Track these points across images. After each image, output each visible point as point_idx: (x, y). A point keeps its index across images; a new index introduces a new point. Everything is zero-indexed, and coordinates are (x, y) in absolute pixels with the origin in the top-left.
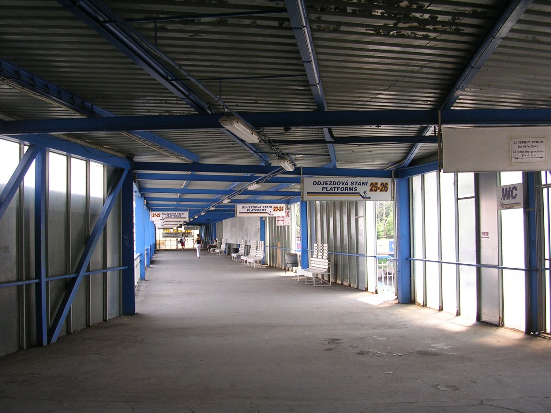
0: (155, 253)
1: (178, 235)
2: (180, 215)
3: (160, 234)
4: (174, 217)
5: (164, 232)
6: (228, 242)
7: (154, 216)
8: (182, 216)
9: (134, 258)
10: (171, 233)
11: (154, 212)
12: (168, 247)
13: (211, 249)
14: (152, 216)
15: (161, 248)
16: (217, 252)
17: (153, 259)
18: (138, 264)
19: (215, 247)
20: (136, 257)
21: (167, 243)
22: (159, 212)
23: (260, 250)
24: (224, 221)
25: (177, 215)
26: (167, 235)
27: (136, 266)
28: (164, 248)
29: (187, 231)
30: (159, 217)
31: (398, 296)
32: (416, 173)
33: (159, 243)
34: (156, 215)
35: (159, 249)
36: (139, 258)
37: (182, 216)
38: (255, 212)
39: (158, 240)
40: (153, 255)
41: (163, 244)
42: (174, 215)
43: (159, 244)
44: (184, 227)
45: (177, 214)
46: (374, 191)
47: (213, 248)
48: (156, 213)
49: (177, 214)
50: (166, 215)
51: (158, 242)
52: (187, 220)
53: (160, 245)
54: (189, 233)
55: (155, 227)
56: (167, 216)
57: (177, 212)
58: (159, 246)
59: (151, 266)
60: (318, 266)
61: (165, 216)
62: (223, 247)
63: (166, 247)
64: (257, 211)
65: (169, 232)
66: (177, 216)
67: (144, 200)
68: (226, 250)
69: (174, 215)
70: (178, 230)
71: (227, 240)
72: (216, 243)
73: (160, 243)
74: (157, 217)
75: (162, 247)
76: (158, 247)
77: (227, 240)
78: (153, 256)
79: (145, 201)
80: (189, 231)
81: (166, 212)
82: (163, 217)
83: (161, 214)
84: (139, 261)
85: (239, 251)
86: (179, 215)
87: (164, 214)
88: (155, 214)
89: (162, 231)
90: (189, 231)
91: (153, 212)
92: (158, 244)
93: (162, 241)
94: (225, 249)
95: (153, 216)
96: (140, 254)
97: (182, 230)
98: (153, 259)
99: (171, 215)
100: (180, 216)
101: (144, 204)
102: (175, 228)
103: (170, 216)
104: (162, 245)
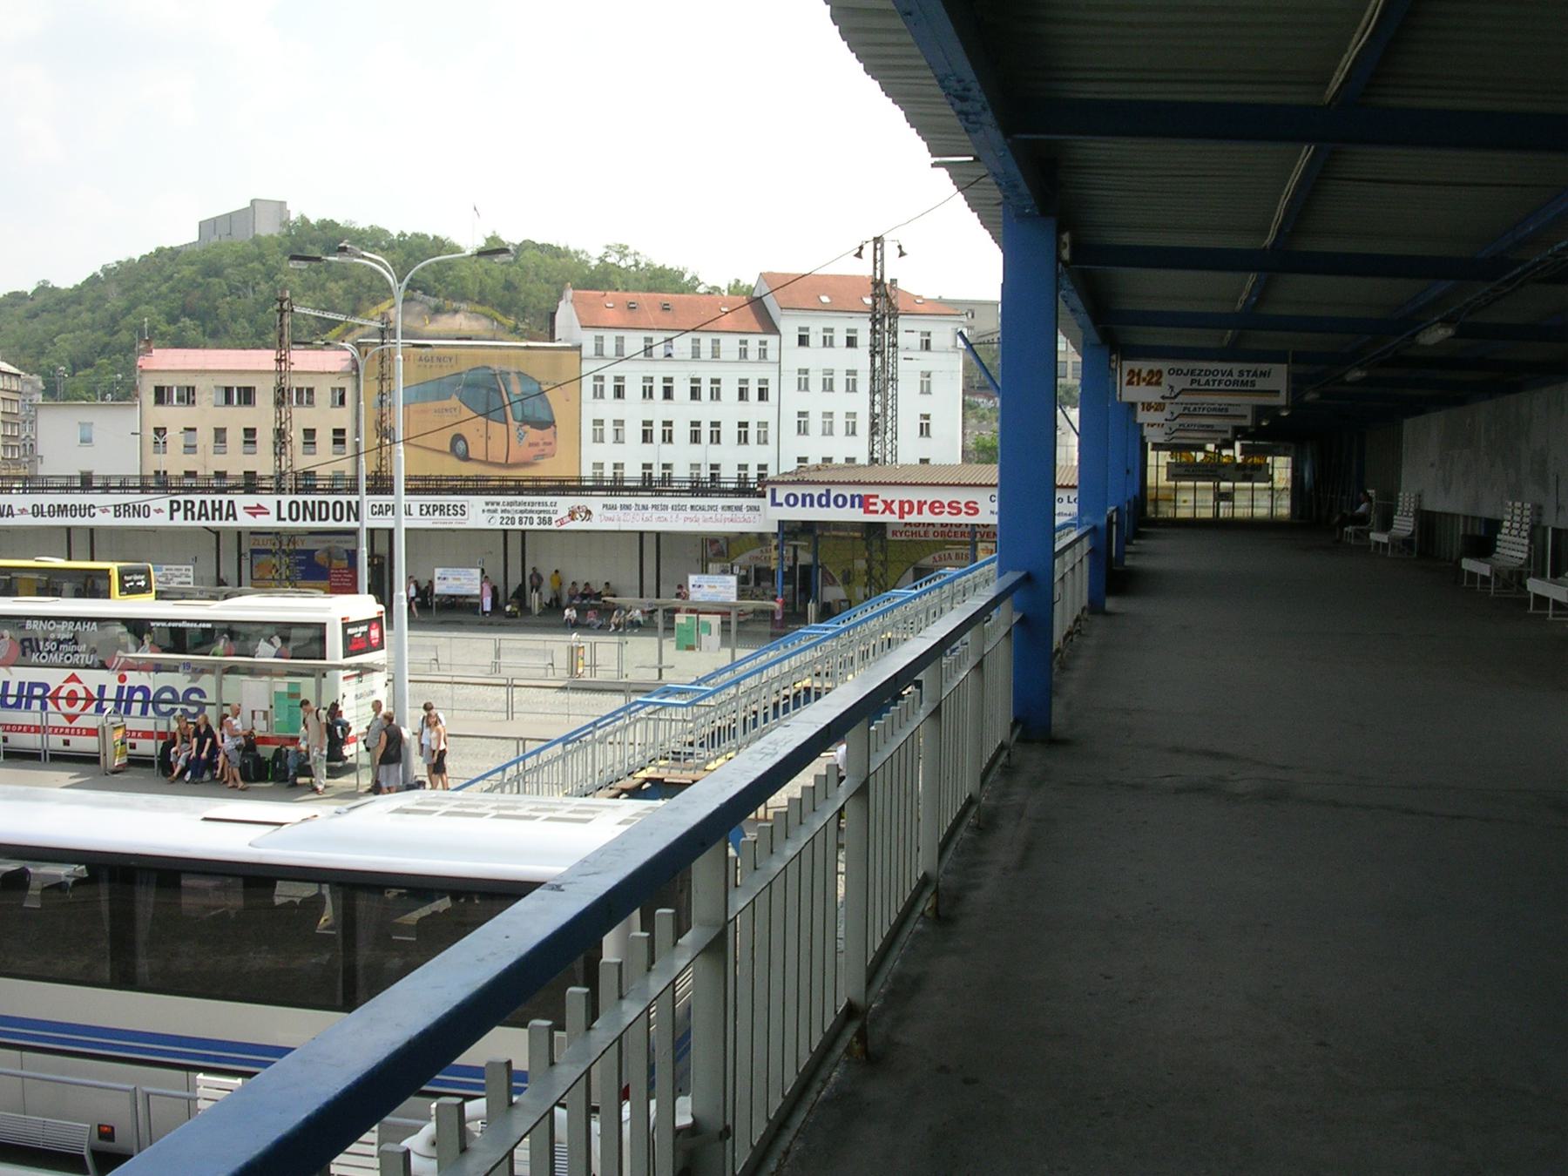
0: (1138, 535)
1: (1221, 471)
2: (1250, 379)
3: (1158, 464)
4: (1222, 387)
5: (1174, 461)
6: (1428, 506)
7: (1135, 379)
8: (1261, 384)
9: (360, 1136)
10: (1195, 464)
11: (1136, 365)
12: (1184, 513)
13: (1349, 529)
14: (1126, 379)
15: (1161, 513)
16: (1378, 543)
17: (1127, 563)
18: (1081, 561)
19: (1363, 520)
20: (367, 1140)
21: (1181, 497)
22: (1156, 365)
23: (1514, 532)
24: (1408, 424)
25: (1236, 377)
26: (1181, 471)
27: (1062, 579)
28: (1170, 514)
29: (1250, 460)
30: (1158, 383)
31: (419, 289)
32: (1270, 455)
33: (1154, 497)
34: (1144, 374)
35: (1153, 516)
36: (1086, 541)
37: (1261, 384)
38: (1216, 387)
39: (1153, 488)
40: (1129, 543)
41: (1170, 500)
42: (1225, 378)
43: (1156, 501)
44: (1242, 445)
45: (1235, 373)
46: (181, 669)
47: (1354, 525)
48: (1144, 366)
49: (1235, 373)
50: (1189, 378)
51: (1151, 494)
52: (1247, 422)
53: (1160, 503)
54: (1258, 468)
55: (1143, 438)
56: (1192, 382)
57: (1236, 367)
58: (1156, 507)
59: (1110, 604)
60: (1513, 553)
61: (1182, 382)
62: (1404, 525)
63: (1178, 511)
64: (1205, 412)
65: (1192, 460)
66: (1235, 382)
67: (1111, 355)
68: (1416, 538)
69: (1225, 378)
70: (1220, 454)
71: (1419, 496)
72: (1369, 508)
73: (1159, 497)
74: (1149, 383)
75: (1166, 511)
76: (1150, 509)
77: (1419, 496)
78: (1129, 548)
79: (1066, 238)
80: (1256, 460)
81: (1185, 366)
82: (1171, 387)
83: (1165, 373)
84: (1086, 551)
85: (1498, 550)
86: (1245, 378)
87: (1178, 372)
88: (1139, 374)
89: (1165, 457)
90: (1256, 460)
91: (1128, 365)
92: (1152, 500)
93: (1167, 492)
94: (1413, 534)
95: (1130, 383)
96: (1018, 575)
97: (1236, 453)
98: (1127, 563)
99: (1211, 377)
100: (1253, 383)
101: (1059, 258)
102: (1210, 447)
103: (1207, 383)
104: (1165, 503)
